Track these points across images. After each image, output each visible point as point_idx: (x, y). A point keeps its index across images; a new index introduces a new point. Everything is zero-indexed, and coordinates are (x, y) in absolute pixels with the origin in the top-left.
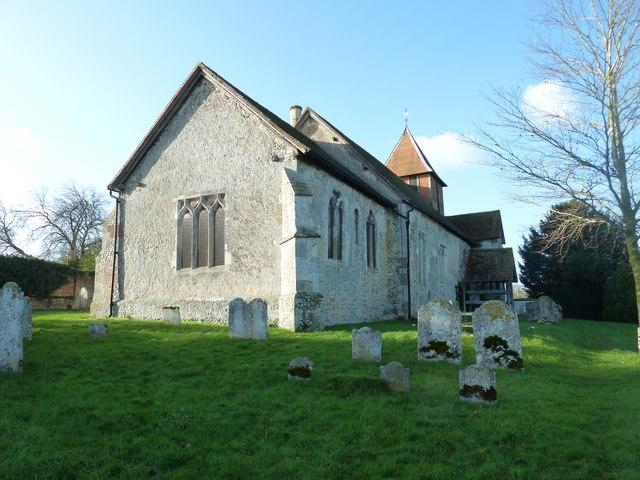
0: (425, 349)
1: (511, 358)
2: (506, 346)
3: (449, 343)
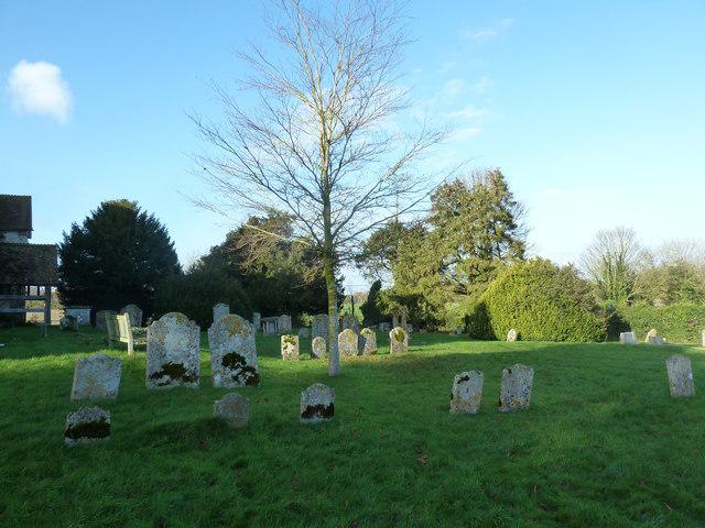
0: (157, 375)
1: (249, 374)
2: (244, 363)
3: (186, 365)
